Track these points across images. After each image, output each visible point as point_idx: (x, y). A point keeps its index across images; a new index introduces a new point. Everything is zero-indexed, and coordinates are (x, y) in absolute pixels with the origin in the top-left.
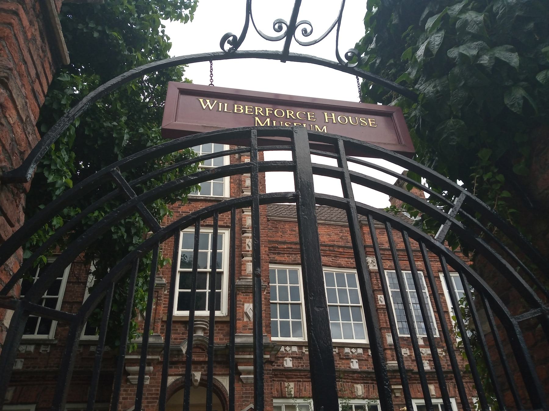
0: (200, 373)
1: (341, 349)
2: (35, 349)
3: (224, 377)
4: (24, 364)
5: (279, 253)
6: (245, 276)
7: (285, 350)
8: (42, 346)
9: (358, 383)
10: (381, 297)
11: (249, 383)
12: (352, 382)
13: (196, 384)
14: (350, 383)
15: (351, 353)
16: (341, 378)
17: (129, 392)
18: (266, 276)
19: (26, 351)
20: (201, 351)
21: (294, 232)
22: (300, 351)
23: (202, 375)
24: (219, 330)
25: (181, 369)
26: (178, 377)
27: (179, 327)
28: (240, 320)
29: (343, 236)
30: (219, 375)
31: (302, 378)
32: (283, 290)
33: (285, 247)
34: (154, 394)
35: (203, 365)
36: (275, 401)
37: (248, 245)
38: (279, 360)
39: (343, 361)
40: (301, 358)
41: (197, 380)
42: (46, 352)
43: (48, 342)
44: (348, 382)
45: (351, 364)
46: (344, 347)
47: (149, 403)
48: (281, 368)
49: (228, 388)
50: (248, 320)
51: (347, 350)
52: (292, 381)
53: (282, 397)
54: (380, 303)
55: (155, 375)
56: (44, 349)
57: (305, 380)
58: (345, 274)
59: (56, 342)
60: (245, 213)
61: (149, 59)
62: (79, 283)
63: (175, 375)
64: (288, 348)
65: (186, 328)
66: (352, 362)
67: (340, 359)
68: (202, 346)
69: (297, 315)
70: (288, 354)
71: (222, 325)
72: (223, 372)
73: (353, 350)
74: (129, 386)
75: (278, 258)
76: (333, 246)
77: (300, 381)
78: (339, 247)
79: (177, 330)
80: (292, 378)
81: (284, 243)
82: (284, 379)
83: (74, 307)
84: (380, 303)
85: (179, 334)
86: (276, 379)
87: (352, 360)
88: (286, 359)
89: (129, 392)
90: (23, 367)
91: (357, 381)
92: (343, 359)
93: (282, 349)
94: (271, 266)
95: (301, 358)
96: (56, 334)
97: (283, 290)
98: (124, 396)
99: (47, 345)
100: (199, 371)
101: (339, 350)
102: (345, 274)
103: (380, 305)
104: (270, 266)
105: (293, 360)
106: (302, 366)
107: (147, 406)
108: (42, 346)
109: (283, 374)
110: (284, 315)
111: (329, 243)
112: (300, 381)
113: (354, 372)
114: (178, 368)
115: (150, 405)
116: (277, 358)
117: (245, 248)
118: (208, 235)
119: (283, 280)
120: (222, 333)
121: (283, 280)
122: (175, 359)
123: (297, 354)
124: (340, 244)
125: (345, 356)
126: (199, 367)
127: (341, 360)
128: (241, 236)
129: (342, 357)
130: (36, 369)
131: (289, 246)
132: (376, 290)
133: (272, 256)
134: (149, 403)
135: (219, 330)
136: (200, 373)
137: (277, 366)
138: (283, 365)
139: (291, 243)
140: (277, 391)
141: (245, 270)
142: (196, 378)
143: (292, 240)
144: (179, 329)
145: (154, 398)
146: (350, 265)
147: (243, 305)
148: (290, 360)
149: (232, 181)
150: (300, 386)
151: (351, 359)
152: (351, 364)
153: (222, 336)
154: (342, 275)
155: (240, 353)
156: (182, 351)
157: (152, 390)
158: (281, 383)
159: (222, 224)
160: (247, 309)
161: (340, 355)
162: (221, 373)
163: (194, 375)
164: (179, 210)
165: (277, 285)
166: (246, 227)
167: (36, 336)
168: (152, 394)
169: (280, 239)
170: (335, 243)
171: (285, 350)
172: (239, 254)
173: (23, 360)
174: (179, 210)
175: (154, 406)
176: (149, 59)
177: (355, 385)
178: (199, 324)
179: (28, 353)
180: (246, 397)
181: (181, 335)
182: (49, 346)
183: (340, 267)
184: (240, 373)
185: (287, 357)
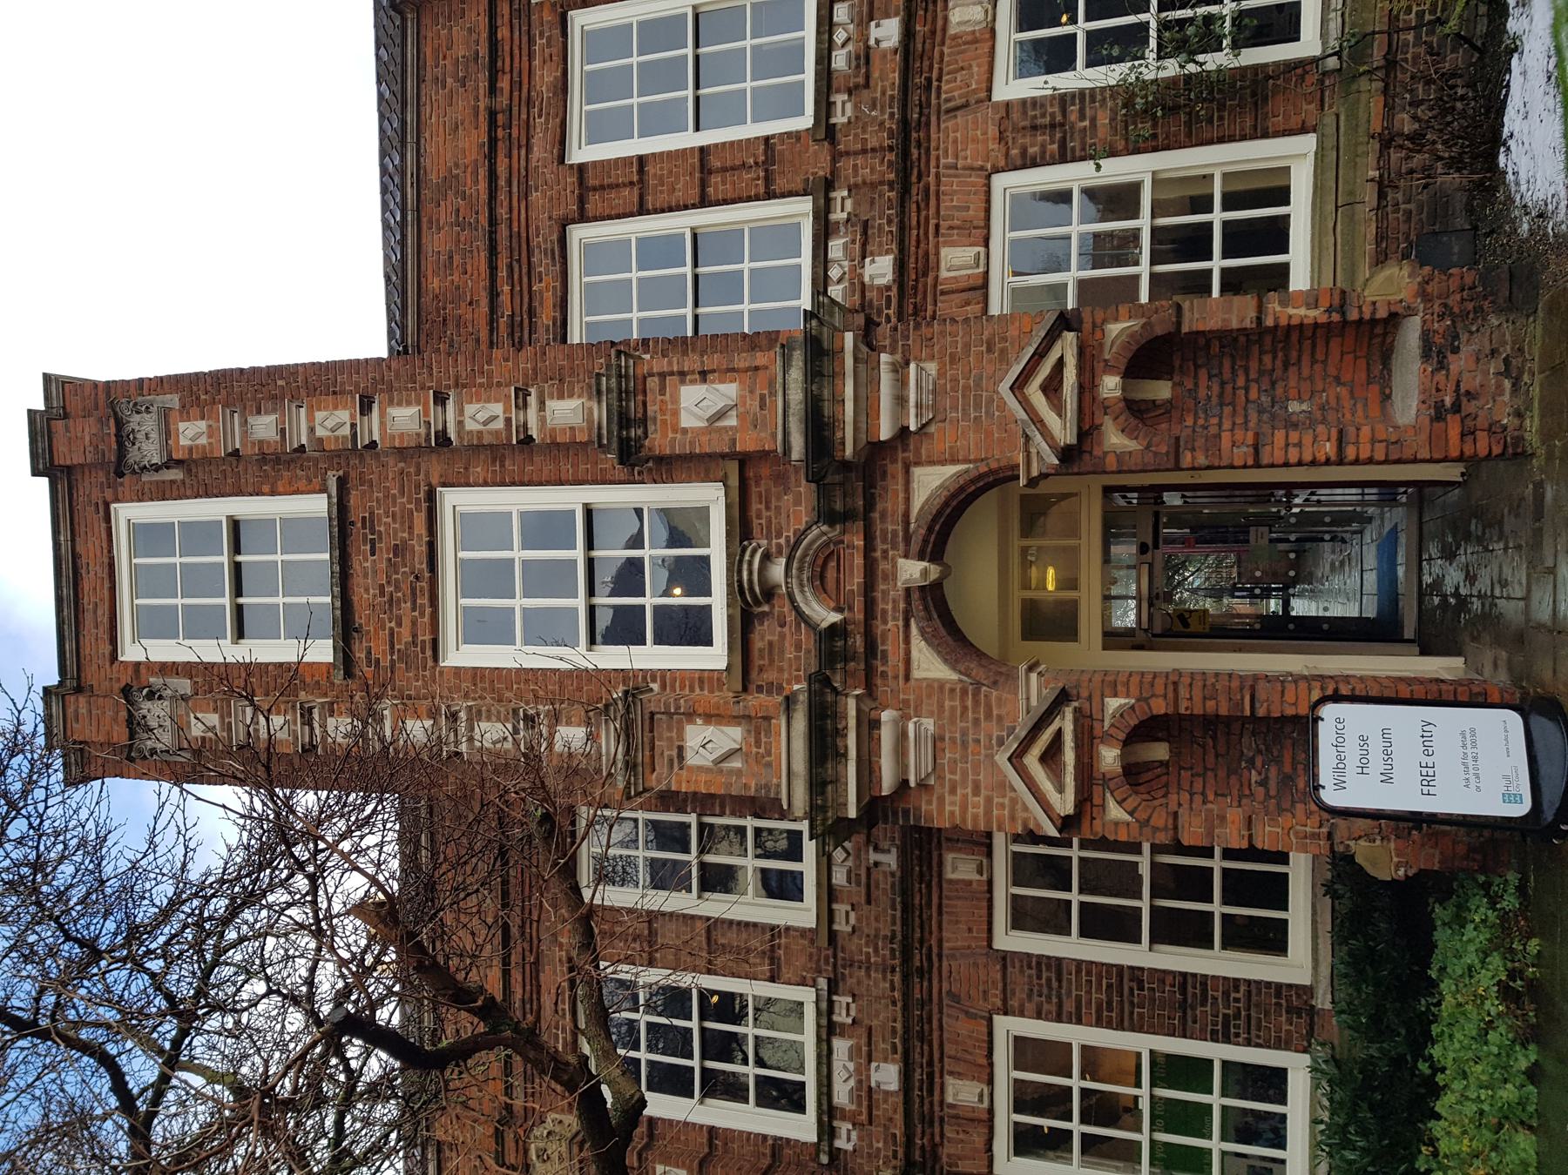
1: (835, 84)
2: (842, 1035)
3: (915, 485)
4: (886, 1060)
5: (532, 313)
6: (590, 429)
7: (839, 281)
8: (835, 1018)
9: (946, 19)
11: (935, 400)
12: (943, 43)
13: (935, 571)
14: (946, 51)
15: (850, 47)
16: (929, 80)
17: (957, 777)
18: (590, 354)
19: (851, 1059)
20: (833, 564)
21: (456, 258)
22: (842, 229)
23: (906, 556)
24: (768, 508)
25: (890, 624)
26: (914, 630)
27: (762, 639)
28: (734, 441)
30: (908, 500)
31: (927, 219)
32: (652, 293)
33: (506, 288)
34: (963, 700)
35: (878, 554)
36: (994, 310)
37: (485, 423)
39: (876, 74)
40: (865, 225)
41: (925, 573)
42: (853, 1006)
43: (824, 1005)
44: (942, 54)
45: (884, 45)
46: (829, 72)
47: (989, 716)
48: (894, 293)
49: (951, 470)
50: (734, 413)
51: (840, 61)
52: (937, 254)
53: (983, 285)
55: (906, 702)
56: (844, 1013)
57: (932, 211)
58: (587, 68)
59: (823, 983)
60: (376, 437)
62: (652, 932)
63: (907, 640)
64: (834, 273)
65: (764, 614)
66: (877, 42)
67: (867, 86)
68: (820, 562)
69: (728, 243)
70: (853, 269)
71: (754, 498)
72: (900, 487)
73: (840, 36)
74: (941, 778)
75: (546, 316)
76: (492, 114)
77: (937, 226)
78: (493, 90)
79: (771, 644)
80: (927, 254)
81: (494, 294)
82: (930, 280)
83: (722, 941)
85: (782, 636)
86: (930, 308)
87: (872, 42)
88: (867, 279)
89: (957, 777)
90: (894, 1061)
91: (940, 23)
92: (867, 77)
93: (836, 292)
94: (576, 336)
95: (865, 225)
96: (802, 983)
97: (652, 293)
98: (969, 790)
99: (831, 1003)
100: (895, 566)
101: (838, 91)
102: (587, 68)
104: (576, 341)
105: (872, 254)
106: (890, 222)
107: (1000, 718)
108: (835, 1018)
109: (915, 288)
110: (730, 288)
111: (484, 127)
112: (937, 226)
113: (908, 33)
114: (884, 634)
115: (995, 713)
116: (864, 306)
117: (497, 432)
118: (462, 560)
119: (617, 296)
120: (779, 499)
121: (617, 296)
122: (859, 642)
123: (853, 242)
124: (483, 85)
125: (858, 66)
126: (883, 566)
127: (872, 84)
128: (457, 450)
129: (861, 80)
130: (899, 1026)
131: (503, 273)
133: (541, 336)
134: (989, 716)
135: (768, 508)
136: (901, 561)
137: (888, 307)
138: (888, 288)
139: (493, 269)
140: (968, 303)
142: (917, 575)
143: (484, 266)
144: (768, 638)
145: (976, 703)
146: (554, 50)
147: (685, 431)
148: (873, 261)
149: (266, 488)
150: (951, 228)
151: (868, 47)
152: (884, 45)
153: (788, 498)
154: (589, 78)
155: (839, 435)
156: (833, 626)
157: (953, 708)
158: (943, 293)
159: (423, 515)
160: (699, 418)
161: (857, 87)
162: (901, 495)
163: (907, 581)
164: (385, 662)
165: (635, 315)
166: (423, 431)
167: (808, 1038)
168: (965, 708)
169: (484, 308)
170: (482, 105)
171: (839, 281)
172: (522, 451)
173: (874, 1065)
174: (385, 662)
175: (999, 699)
177: (952, 31)
178: (750, 581)
179: (853, 1053)
180: (978, 406)
181: (786, 630)
182: (835, 998)
183: (563, 87)
184: (903, 432)
185: (861, 276)
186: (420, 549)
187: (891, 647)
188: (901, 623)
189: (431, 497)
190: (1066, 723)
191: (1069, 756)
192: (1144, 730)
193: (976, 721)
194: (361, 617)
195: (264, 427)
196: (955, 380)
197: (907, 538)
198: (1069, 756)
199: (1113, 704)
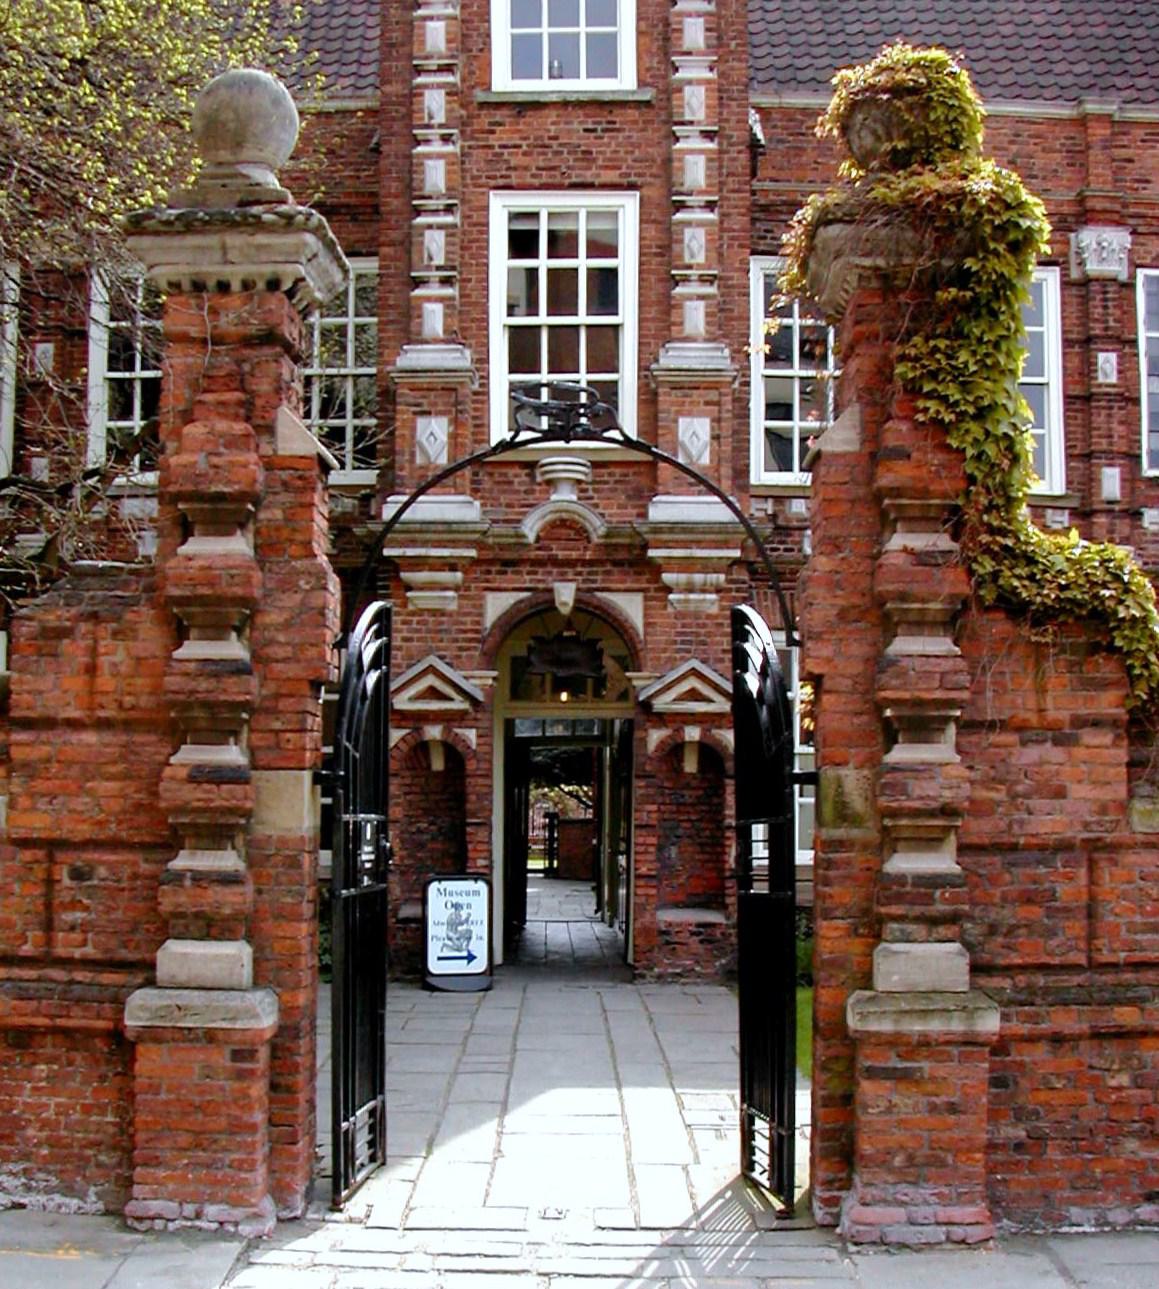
0: (573, 586)
10: (1107, 361)
23: (578, 590)
25: (527, 577)
29: (1018, 155)
34: (472, 631)
35: (579, 569)
38: (790, 535)
54: (1101, 379)
61: (555, 863)
84: (1101, 379)
103: (1100, 385)
115: (464, 654)
132: (1097, 337)
135: (616, 482)
136: (573, 586)
141: (681, 324)
145: (471, 640)
164: (493, 140)
166: (684, 189)
168: (465, 632)
174: (493, 140)
175: (470, 657)
176: (555, 863)
180: (683, 642)
186: (588, 176)
187: (510, 578)
188: (528, 585)
189: (632, 187)
190: (459, 704)
191: (435, 705)
192: (454, 753)
193: (456, 640)
194: (532, 119)
195: (694, 34)
196: (704, 626)
197: (591, 590)
198: (435, 705)
199: (471, 735)
